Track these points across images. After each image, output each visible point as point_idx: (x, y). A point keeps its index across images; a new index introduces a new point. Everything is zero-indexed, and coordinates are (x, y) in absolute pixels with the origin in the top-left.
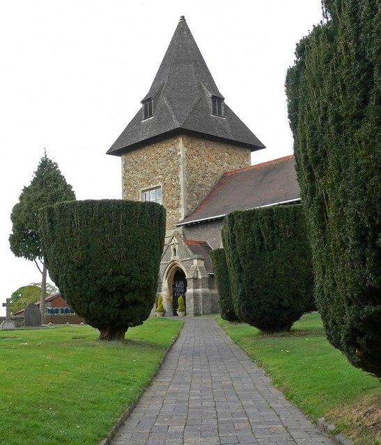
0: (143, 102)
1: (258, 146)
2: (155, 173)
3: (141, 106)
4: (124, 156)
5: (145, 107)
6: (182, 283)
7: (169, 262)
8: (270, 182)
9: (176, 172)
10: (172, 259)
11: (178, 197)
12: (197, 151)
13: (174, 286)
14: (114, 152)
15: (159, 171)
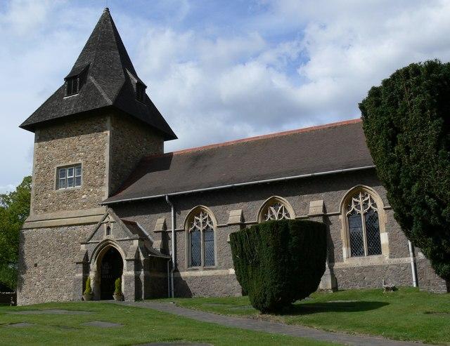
0: (67, 79)
1: (172, 136)
2: (76, 150)
3: (63, 82)
4: (38, 132)
5: (69, 85)
6: (267, 304)
7: (101, 241)
8: (206, 166)
9: (101, 150)
10: (105, 237)
11: (103, 176)
12: (122, 132)
13: (101, 267)
14: (27, 126)
15: (80, 148)
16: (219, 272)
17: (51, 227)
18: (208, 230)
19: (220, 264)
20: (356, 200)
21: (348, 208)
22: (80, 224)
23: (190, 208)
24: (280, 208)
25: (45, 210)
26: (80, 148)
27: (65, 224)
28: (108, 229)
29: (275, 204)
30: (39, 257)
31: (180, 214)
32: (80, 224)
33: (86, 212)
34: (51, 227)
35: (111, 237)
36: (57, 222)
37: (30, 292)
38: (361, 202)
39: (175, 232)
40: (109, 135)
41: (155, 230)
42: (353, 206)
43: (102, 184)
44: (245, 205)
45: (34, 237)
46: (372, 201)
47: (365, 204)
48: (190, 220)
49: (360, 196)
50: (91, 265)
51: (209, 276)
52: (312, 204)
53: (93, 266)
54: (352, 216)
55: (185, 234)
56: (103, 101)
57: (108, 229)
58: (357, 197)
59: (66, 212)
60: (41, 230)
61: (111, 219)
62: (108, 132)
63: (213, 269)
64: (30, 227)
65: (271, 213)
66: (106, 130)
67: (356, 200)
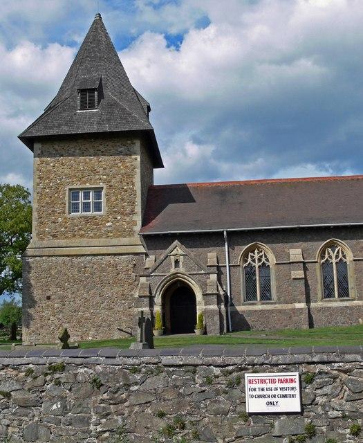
2: (95, 172)
7: (168, 274)
9: (130, 176)
10: (173, 270)
15: (101, 170)
16: (278, 306)
17: (68, 256)
18: (264, 267)
19: (279, 299)
20: (252, 254)
21: (323, 257)
22: (109, 255)
23: (324, 240)
24: (337, 250)
25: (54, 236)
26: (101, 170)
27: (89, 253)
28: (177, 262)
29: (332, 246)
30: (53, 289)
31: (233, 249)
32: (109, 255)
33: (114, 241)
34: (68, 256)
35: (181, 269)
36: (132, 248)
37: (42, 327)
38: (256, 256)
39: (230, 266)
40: (139, 159)
41: (209, 264)
42: (249, 260)
43: (132, 212)
44: (304, 245)
45: (45, 266)
46: (266, 256)
47: (260, 260)
48: (245, 256)
49: (256, 251)
50: (156, 298)
51: (269, 310)
52: (292, 252)
53: (158, 299)
54: (326, 266)
55: (317, 266)
56: (94, 118)
57: (177, 262)
58: (253, 252)
59: (85, 239)
60: (54, 258)
61: (180, 252)
62: (139, 158)
63: (347, 300)
64: (37, 254)
65: (329, 254)
66: (135, 154)
67: (252, 254)
